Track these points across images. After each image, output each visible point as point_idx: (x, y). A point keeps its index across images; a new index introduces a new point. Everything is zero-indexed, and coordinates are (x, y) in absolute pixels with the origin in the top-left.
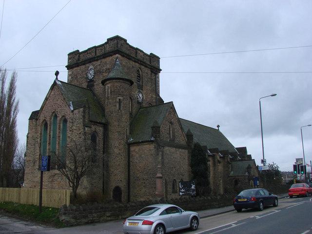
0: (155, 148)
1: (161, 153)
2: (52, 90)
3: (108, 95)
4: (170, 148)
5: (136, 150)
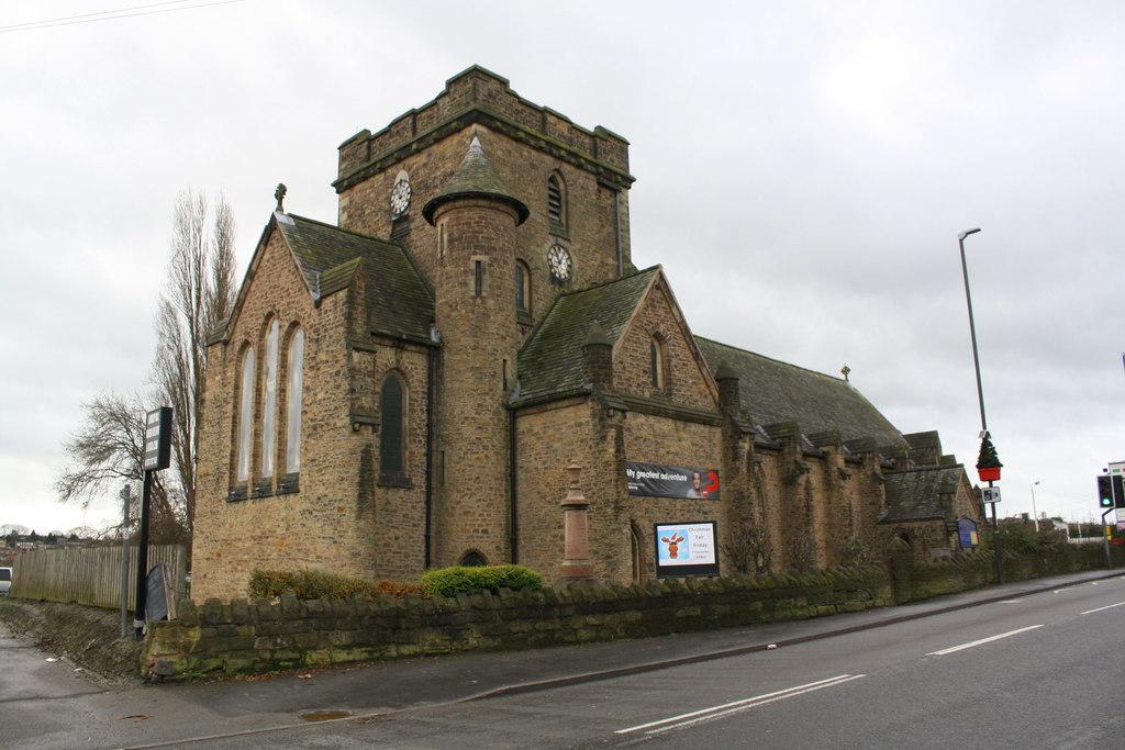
0: (594, 416)
1: (612, 433)
2: (266, 245)
3: (442, 252)
4: (652, 420)
5: (536, 430)
